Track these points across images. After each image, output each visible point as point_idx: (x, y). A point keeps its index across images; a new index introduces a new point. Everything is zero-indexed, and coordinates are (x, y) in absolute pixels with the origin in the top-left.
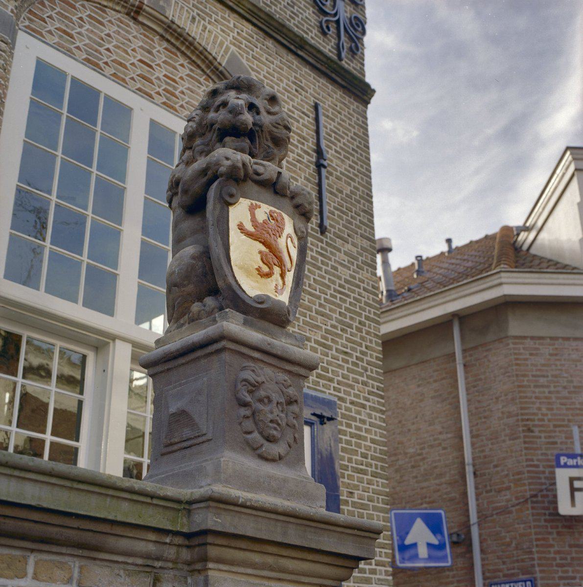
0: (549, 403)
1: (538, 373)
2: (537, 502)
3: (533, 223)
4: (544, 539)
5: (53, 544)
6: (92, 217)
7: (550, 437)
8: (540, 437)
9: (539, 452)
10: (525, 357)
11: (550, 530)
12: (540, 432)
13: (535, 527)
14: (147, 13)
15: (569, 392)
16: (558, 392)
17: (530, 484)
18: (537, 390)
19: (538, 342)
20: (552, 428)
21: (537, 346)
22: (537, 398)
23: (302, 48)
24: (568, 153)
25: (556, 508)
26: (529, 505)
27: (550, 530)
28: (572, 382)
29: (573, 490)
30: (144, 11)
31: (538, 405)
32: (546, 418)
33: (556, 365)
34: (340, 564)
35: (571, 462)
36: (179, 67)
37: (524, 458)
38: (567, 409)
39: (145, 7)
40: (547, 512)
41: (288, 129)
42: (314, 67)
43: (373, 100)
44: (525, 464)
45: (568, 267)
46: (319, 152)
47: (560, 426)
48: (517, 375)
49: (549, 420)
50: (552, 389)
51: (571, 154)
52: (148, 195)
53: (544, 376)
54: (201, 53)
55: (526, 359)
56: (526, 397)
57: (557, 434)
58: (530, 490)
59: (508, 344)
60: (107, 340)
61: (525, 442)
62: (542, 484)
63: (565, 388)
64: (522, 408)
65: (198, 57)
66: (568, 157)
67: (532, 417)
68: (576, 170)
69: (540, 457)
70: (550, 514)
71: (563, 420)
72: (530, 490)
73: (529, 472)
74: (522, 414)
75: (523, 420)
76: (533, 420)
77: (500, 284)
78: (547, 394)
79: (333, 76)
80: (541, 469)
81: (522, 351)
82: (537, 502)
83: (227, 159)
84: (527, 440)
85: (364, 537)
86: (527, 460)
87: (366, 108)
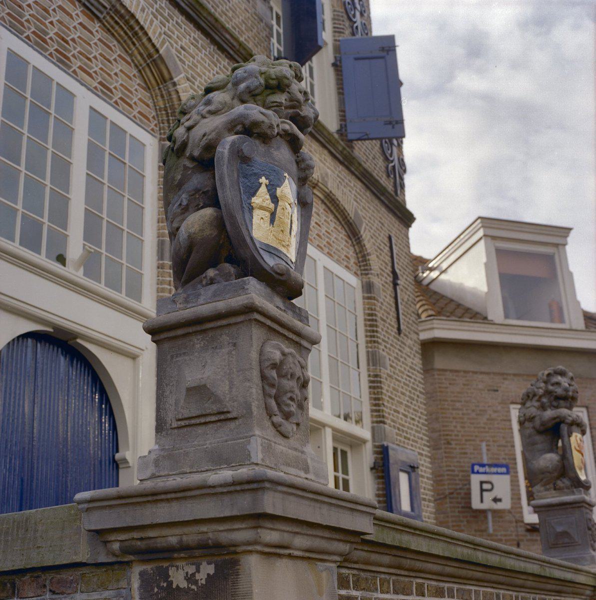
0: (462, 423)
1: (455, 399)
2: (453, 498)
3: (435, 266)
4: (458, 526)
5: (373, 565)
6: (48, 225)
7: (462, 449)
8: (455, 449)
9: (455, 460)
10: (445, 386)
11: (461, 519)
12: (456, 444)
13: (452, 517)
14: (320, 188)
15: (477, 415)
16: (468, 414)
17: (449, 484)
18: (454, 412)
19: (455, 374)
20: (464, 442)
21: (454, 377)
22: (454, 418)
23: (383, 194)
24: (479, 221)
25: (470, 503)
26: (448, 500)
27: (461, 519)
28: (478, 406)
29: (482, 490)
30: (318, 186)
31: (454, 424)
32: (460, 434)
33: (467, 393)
34: (457, 566)
35: (482, 470)
36: (113, 76)
37: (444, 464)
38: (475, 427)
39: (320, 184)
40: (460, 506)
41: (577, 392)
42: (387, 207)
43: (414, 225)
44: (445, 469)
45: (478, 316)
46: (394, 272)
47: (469, 440)
48: (440, 400)
49: (462, 436)
50: (465, 412)
51: (481, 222)
52: (28, 171)
53: (459, 401)
54: (342, 211)
55: (446, 388)
56: (446, 418)
57: (467, 446)
58: (449, 489)
59: (434, 375)
60: (320, 427)
61: (445, 452)
62: (456, 484)
63: (473, 411)
64: (444, 426)
65: (339, 214)
66: (478, 224)
67: (450, 433)
68: (485, 235)
69: (456, 464)
70: (462, 507)
71: (472, 436)
72: (449, 489)
73: (448, 475)
74: (444, 431)
75: (444, 435)
76: (451, 435)
77: (433, 328)
78: (461, 416)
79: (396, 211)
80: (456, 473)
81: (444, 381)
82: (453, 498)
83: (570, 416)
84: (447, 450)
85: (486, 552)
86: (447, 466)
87: (408, 230)
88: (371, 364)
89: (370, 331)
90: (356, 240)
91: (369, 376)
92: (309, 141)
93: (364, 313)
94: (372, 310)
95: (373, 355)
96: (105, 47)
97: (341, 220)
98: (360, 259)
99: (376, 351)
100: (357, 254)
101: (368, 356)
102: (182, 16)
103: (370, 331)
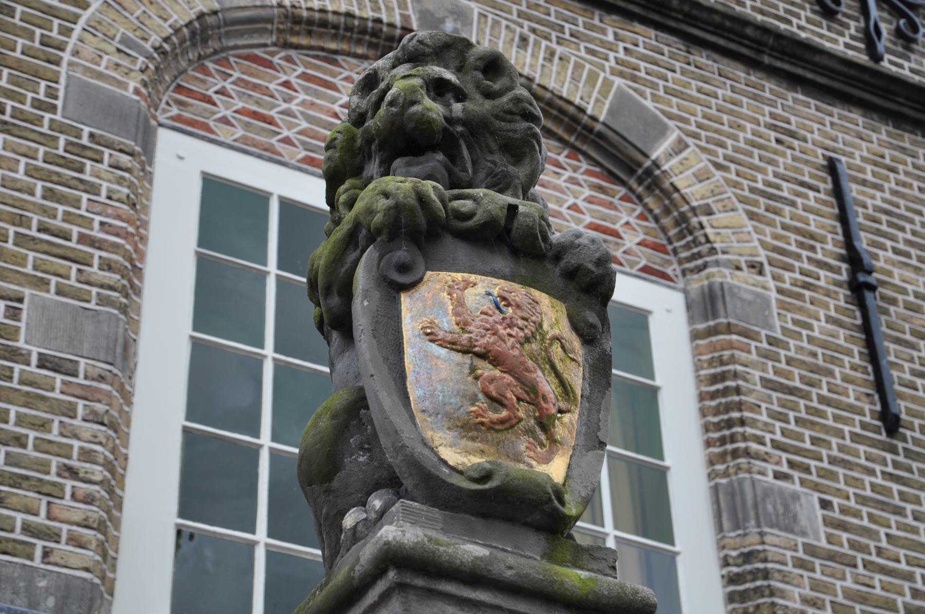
88: (726, 524)
89: (718, 427)
90: (640, 181)
91: (725, 562)
92: (743, 75)
93: (698, 377)
94: (722, 363)
95: (732, 495)
96: (254, 66)
97: (560, 131)
98: (672, 232)
99: (741, 482)
100: (657, 219)
101: (716, 502)
102: (887, 125)
103: (718, 427)
